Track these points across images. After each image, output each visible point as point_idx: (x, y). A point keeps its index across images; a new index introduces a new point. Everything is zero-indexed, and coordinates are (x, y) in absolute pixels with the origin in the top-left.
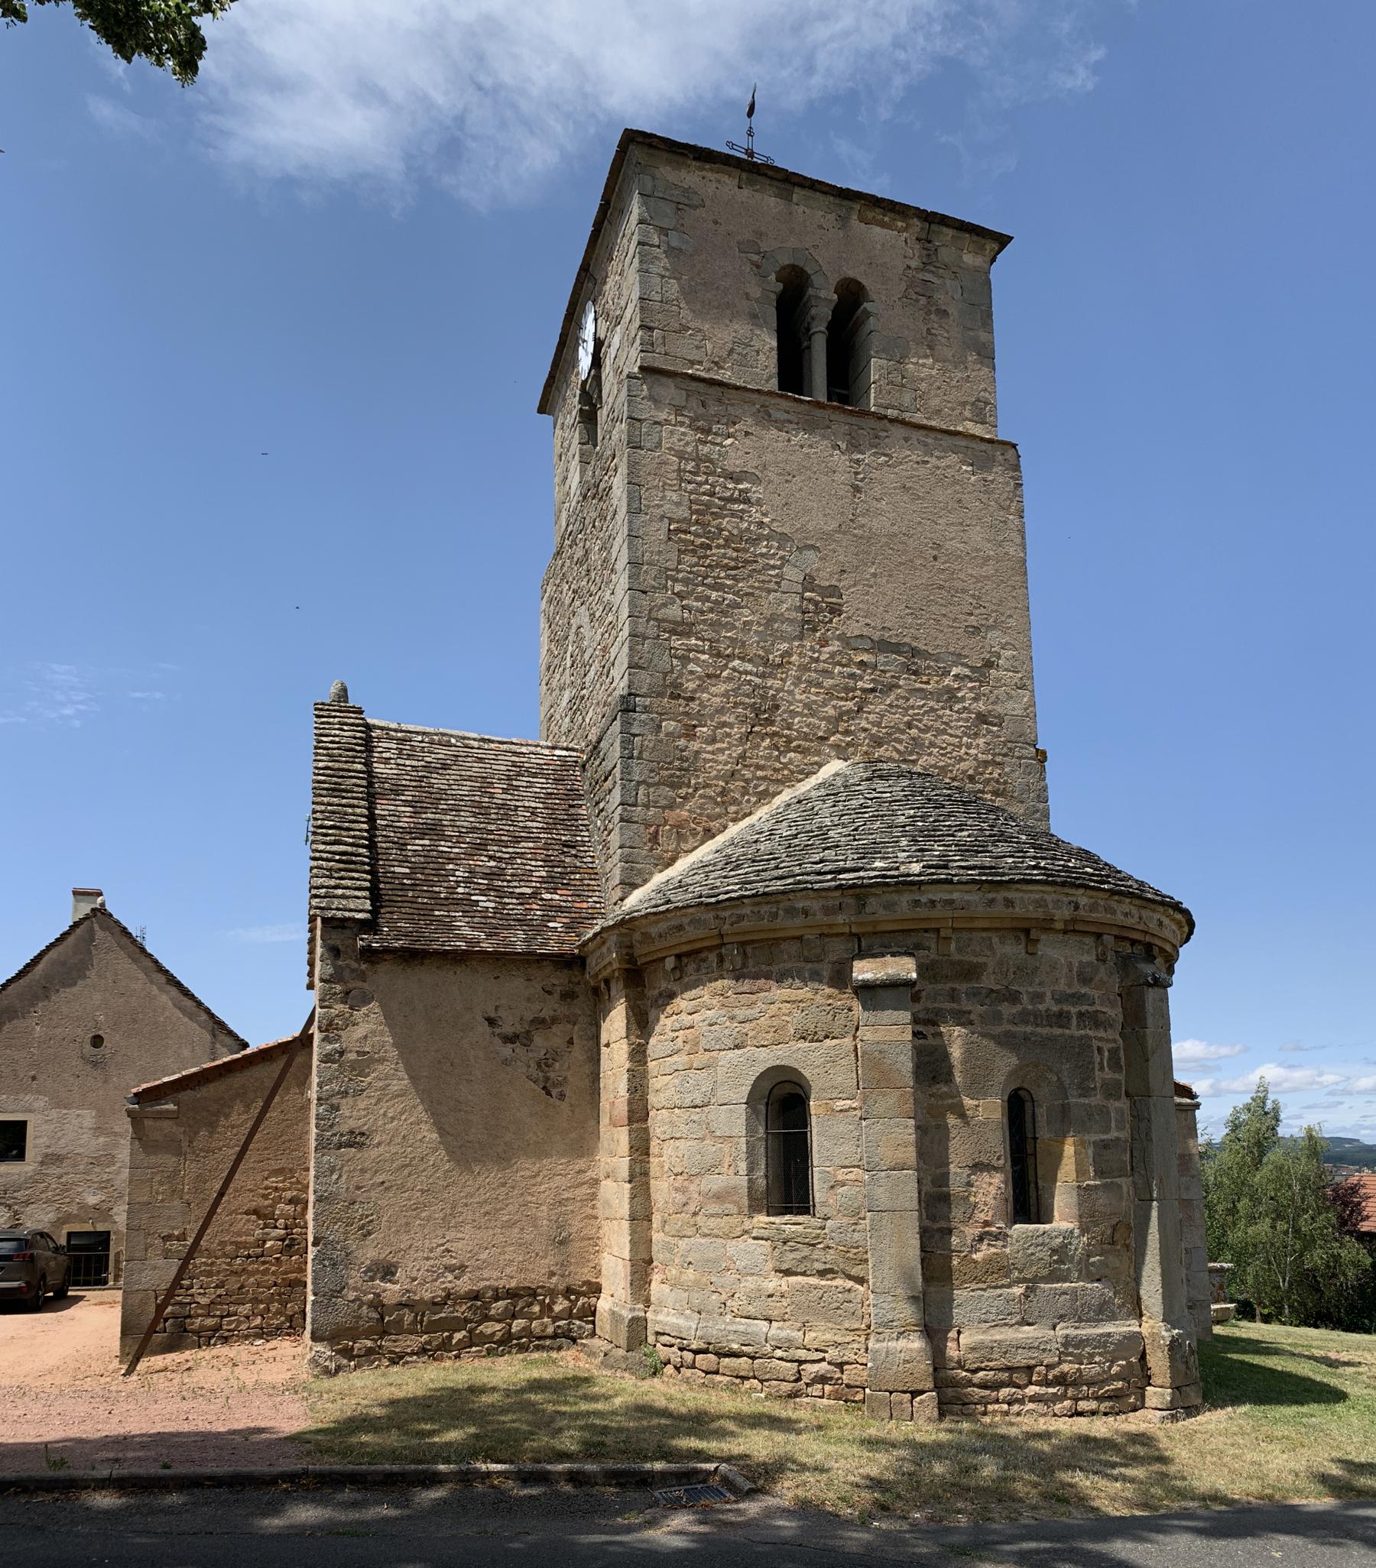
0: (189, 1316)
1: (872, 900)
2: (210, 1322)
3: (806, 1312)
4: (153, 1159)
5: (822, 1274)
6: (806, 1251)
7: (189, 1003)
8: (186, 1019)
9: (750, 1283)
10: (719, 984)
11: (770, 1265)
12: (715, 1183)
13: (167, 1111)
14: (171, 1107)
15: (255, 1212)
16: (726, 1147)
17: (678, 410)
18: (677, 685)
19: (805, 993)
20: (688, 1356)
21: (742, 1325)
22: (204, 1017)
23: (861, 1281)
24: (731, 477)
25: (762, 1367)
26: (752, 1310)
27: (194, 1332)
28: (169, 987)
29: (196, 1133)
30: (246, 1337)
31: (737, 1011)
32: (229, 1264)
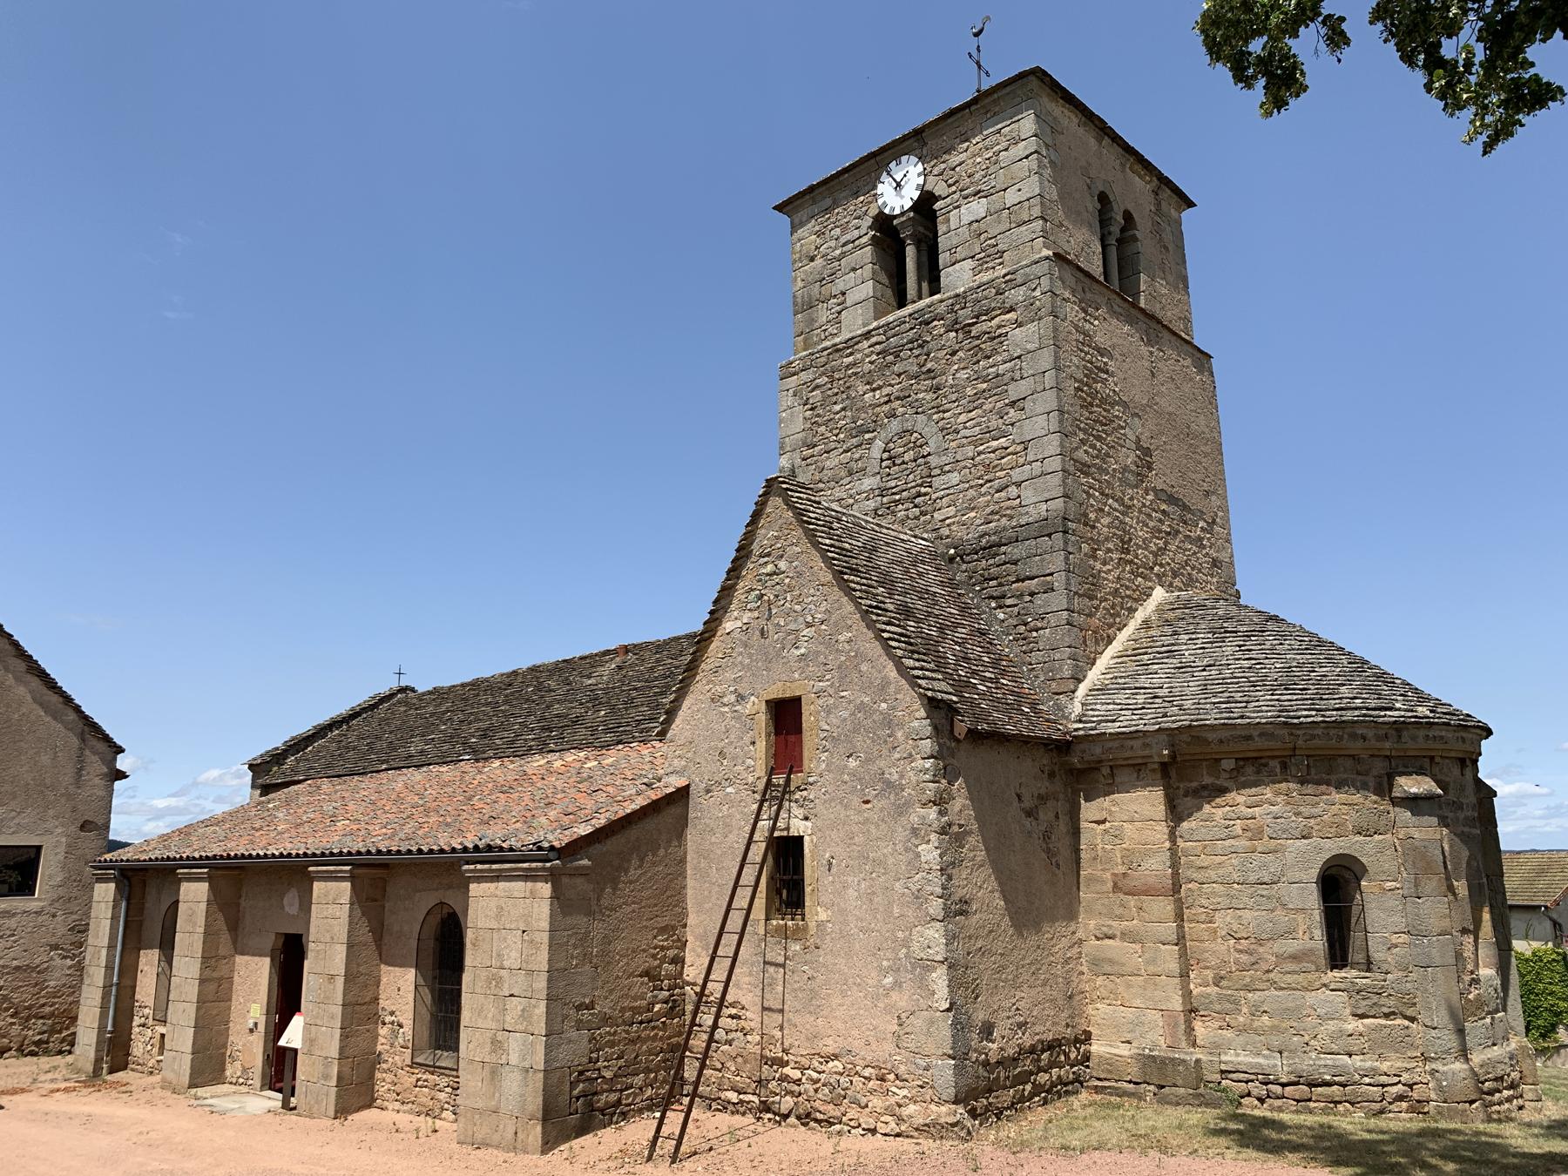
0: (596, 1093)
1: (1405, 733)
2: (613, 1097)
3: (1378, 1045)
4: (569, 920)
5: (1387, 1016)
6: (1375, 998)
7: (55, 698)
8: (48, 719)
9: (1332, 1026)
10: (1284, 785)
11: (1348, 1011)
12: (1292, 946)
13: (584, 867)
14: (585, 862)
15: (646, 973)
16: (1300, 917)
17: (1073, 292)
18: (1086, 515)
19: (1357, 798)
20: (1277, 1089)
21: (1329, 1060)
22: (72, 716)
23: (1412, 1019)
24: (1098, 349)
25: (1354, 1092)
26: (1335, 1048)
27: (602, 1111)
28: (29, 677)
29: (603, 890)
30: (641, 1111)
31: (1302, 809)
32: (627, 1032)
